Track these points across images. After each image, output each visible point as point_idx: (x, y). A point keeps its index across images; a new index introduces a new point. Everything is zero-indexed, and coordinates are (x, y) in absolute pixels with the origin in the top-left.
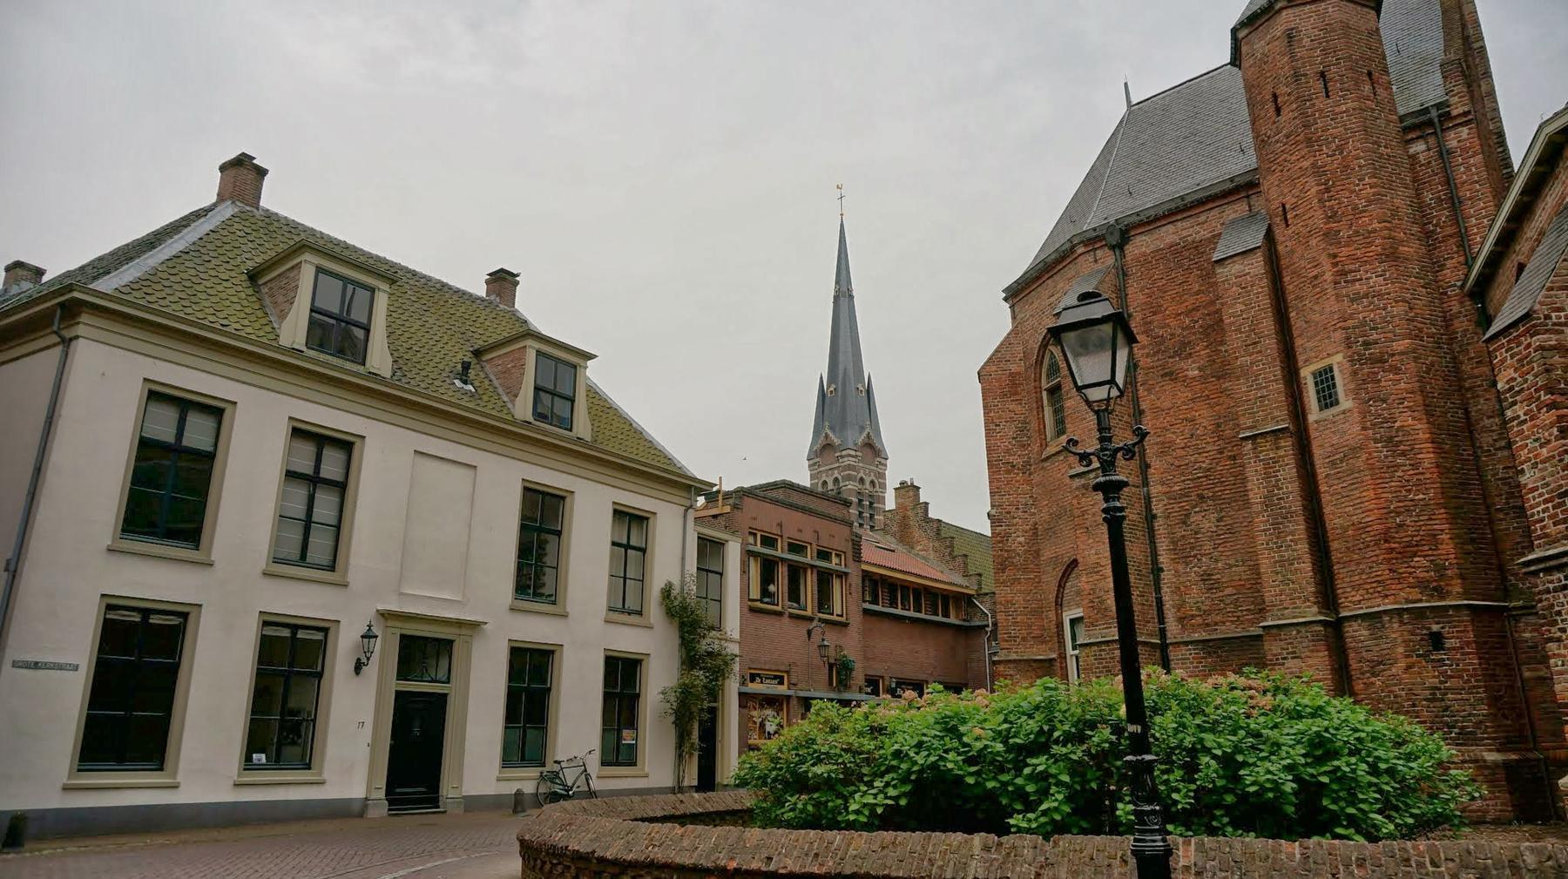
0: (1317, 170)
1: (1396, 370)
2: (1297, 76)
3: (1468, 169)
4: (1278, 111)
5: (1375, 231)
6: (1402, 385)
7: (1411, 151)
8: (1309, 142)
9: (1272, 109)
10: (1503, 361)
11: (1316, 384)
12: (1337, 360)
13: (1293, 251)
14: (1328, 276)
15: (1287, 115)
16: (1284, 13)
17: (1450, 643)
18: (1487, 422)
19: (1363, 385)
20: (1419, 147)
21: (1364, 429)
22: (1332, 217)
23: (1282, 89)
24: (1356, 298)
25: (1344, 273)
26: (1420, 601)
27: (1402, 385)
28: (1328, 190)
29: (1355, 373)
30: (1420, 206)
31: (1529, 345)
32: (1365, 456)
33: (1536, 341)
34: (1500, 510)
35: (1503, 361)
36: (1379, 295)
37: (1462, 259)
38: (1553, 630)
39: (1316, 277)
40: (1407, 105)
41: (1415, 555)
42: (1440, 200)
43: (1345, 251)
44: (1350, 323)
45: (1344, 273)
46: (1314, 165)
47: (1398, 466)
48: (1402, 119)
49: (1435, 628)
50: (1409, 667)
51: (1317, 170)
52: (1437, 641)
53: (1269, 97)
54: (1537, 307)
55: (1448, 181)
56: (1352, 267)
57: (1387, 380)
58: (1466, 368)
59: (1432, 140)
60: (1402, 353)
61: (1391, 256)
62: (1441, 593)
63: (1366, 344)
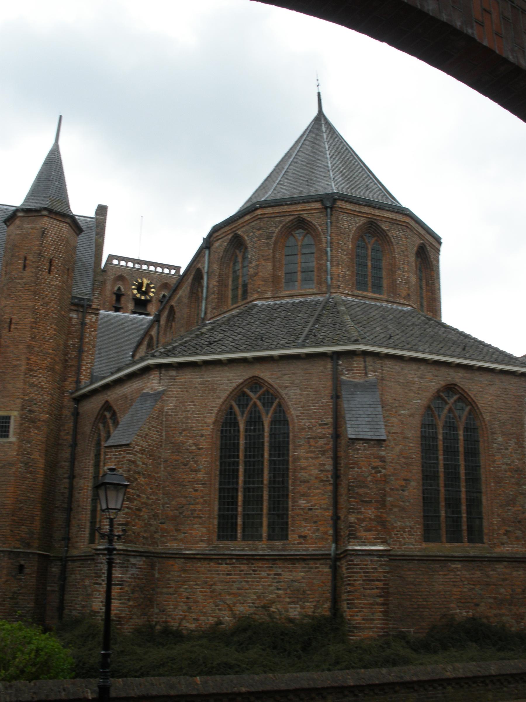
0: (35, 311)
1: (38, 428)
2: (40, 255)
3: (90, 336)
4: (25, 267)
5: (49, 353)
6: (39, 437)
7: (71, 315)
8: (35, 293)
9: (21, 266)
10: (111, 458)
11: (9, 427)
12: (15, 414)
13: (8, 346)
14: (23, 368)
15: (29, 272)
16: (45, 218)
17: (27, 571)
18: (63, 463)
19: (23, 431)
20: (74, 315)
21: (18, 455)
22: (33, 338)
23: (30, 257)
24: (32, 385)
25: (31, 370)
26: (19, 548)
27: (39, 437)
28: (35, 323)
29: (21, 424)
30: (66, 346)
31: (124, 457)
32: (14, 469)
33: (128, 457)
34: (57, 507)
35: (111, 458)
36: (42, 388)
37: (75, 379)
38: (99, 579)
39: (16, 366)
40: (75, 291)
41: (23, 525)
42: (74, 346)
43: (34, 359)
44: (27, 398)
45: (31, 370)
46: (34, 306)
47: (28, 478)
48: (73, 298)
49: (22, 562)
50: (7, 581)
51: (35, 311)
52: (21, 568)
53: (22, 257)
54: (133, 442)
55: (81, 339)
56: (35, 368)
57: (34, 432)
58: (62, 434)
59: (81, 314)
60: (43, 421)
61: (51, 369)
62: (28, 545)
63: (31, 411)
